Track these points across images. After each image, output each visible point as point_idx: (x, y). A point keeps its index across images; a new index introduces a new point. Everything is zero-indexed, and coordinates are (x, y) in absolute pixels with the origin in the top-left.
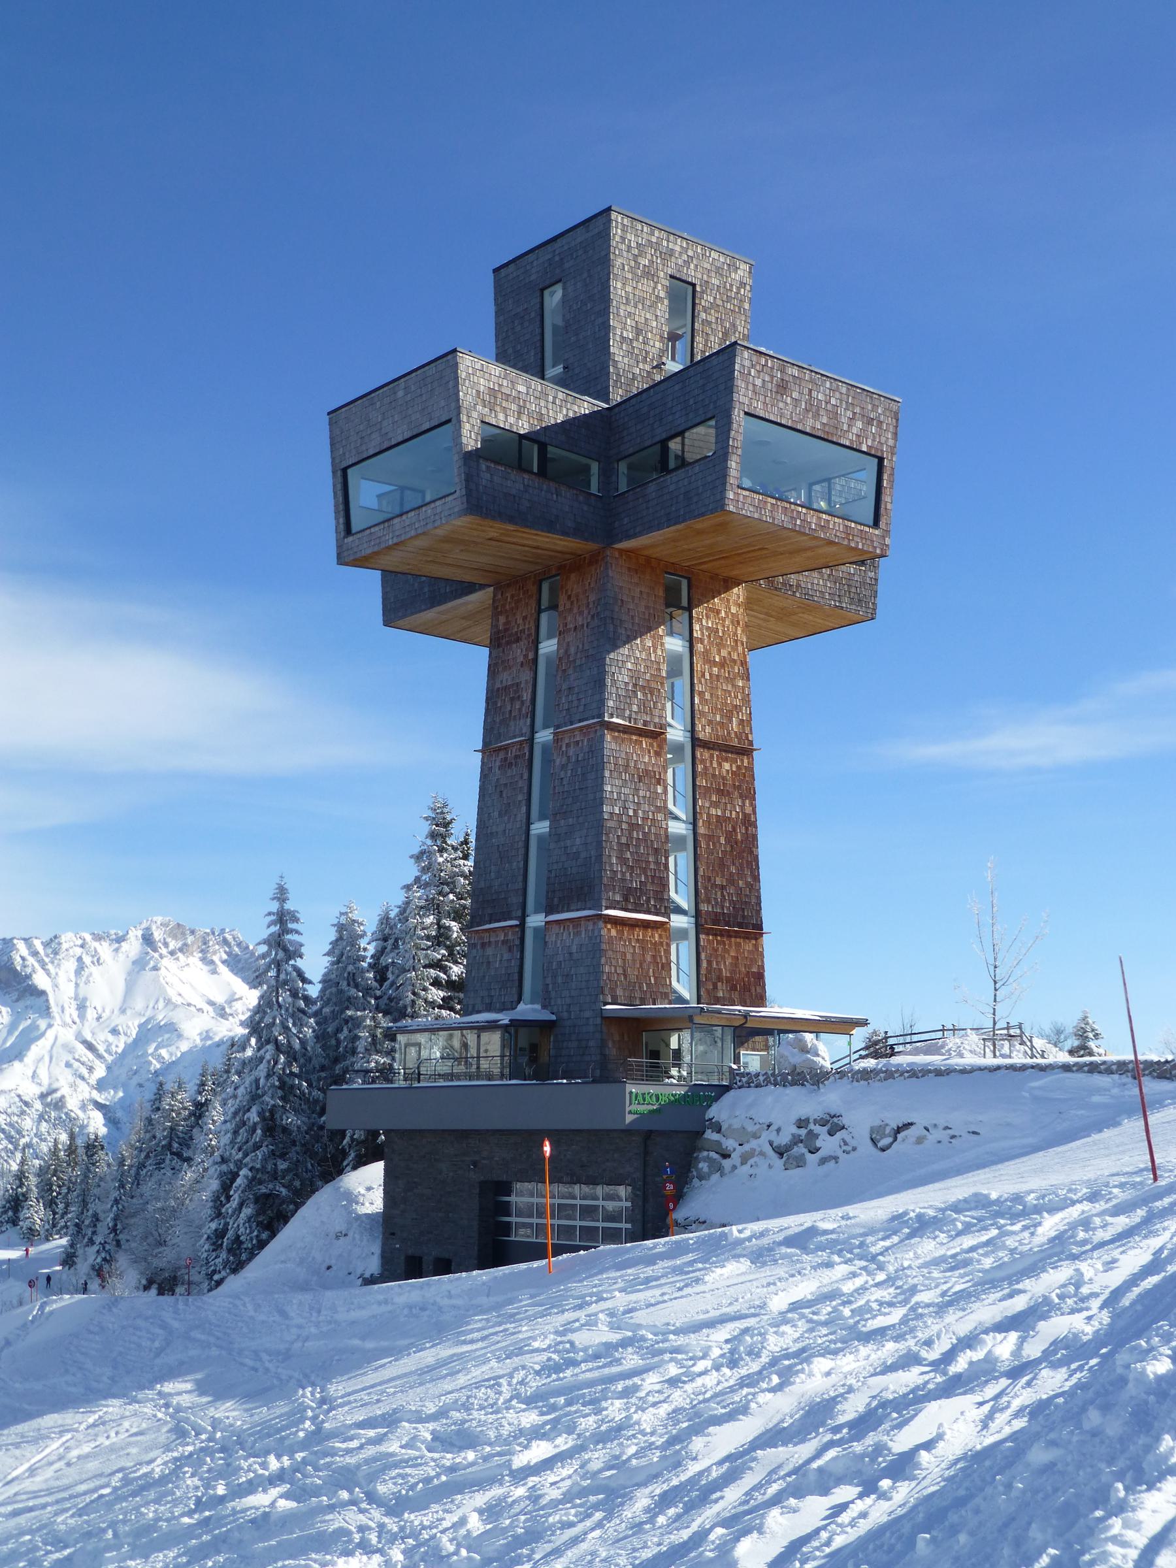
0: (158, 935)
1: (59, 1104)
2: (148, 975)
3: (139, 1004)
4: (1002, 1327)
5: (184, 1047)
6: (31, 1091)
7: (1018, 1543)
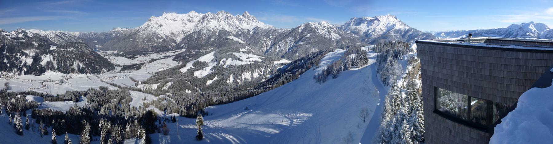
0: (389, 16)
1: (382, 29)
2: (388, 19)
3: (387, 21)
4: (299, 63)
5: (391, 25)
6: (379, 28)
7: (287, 68)
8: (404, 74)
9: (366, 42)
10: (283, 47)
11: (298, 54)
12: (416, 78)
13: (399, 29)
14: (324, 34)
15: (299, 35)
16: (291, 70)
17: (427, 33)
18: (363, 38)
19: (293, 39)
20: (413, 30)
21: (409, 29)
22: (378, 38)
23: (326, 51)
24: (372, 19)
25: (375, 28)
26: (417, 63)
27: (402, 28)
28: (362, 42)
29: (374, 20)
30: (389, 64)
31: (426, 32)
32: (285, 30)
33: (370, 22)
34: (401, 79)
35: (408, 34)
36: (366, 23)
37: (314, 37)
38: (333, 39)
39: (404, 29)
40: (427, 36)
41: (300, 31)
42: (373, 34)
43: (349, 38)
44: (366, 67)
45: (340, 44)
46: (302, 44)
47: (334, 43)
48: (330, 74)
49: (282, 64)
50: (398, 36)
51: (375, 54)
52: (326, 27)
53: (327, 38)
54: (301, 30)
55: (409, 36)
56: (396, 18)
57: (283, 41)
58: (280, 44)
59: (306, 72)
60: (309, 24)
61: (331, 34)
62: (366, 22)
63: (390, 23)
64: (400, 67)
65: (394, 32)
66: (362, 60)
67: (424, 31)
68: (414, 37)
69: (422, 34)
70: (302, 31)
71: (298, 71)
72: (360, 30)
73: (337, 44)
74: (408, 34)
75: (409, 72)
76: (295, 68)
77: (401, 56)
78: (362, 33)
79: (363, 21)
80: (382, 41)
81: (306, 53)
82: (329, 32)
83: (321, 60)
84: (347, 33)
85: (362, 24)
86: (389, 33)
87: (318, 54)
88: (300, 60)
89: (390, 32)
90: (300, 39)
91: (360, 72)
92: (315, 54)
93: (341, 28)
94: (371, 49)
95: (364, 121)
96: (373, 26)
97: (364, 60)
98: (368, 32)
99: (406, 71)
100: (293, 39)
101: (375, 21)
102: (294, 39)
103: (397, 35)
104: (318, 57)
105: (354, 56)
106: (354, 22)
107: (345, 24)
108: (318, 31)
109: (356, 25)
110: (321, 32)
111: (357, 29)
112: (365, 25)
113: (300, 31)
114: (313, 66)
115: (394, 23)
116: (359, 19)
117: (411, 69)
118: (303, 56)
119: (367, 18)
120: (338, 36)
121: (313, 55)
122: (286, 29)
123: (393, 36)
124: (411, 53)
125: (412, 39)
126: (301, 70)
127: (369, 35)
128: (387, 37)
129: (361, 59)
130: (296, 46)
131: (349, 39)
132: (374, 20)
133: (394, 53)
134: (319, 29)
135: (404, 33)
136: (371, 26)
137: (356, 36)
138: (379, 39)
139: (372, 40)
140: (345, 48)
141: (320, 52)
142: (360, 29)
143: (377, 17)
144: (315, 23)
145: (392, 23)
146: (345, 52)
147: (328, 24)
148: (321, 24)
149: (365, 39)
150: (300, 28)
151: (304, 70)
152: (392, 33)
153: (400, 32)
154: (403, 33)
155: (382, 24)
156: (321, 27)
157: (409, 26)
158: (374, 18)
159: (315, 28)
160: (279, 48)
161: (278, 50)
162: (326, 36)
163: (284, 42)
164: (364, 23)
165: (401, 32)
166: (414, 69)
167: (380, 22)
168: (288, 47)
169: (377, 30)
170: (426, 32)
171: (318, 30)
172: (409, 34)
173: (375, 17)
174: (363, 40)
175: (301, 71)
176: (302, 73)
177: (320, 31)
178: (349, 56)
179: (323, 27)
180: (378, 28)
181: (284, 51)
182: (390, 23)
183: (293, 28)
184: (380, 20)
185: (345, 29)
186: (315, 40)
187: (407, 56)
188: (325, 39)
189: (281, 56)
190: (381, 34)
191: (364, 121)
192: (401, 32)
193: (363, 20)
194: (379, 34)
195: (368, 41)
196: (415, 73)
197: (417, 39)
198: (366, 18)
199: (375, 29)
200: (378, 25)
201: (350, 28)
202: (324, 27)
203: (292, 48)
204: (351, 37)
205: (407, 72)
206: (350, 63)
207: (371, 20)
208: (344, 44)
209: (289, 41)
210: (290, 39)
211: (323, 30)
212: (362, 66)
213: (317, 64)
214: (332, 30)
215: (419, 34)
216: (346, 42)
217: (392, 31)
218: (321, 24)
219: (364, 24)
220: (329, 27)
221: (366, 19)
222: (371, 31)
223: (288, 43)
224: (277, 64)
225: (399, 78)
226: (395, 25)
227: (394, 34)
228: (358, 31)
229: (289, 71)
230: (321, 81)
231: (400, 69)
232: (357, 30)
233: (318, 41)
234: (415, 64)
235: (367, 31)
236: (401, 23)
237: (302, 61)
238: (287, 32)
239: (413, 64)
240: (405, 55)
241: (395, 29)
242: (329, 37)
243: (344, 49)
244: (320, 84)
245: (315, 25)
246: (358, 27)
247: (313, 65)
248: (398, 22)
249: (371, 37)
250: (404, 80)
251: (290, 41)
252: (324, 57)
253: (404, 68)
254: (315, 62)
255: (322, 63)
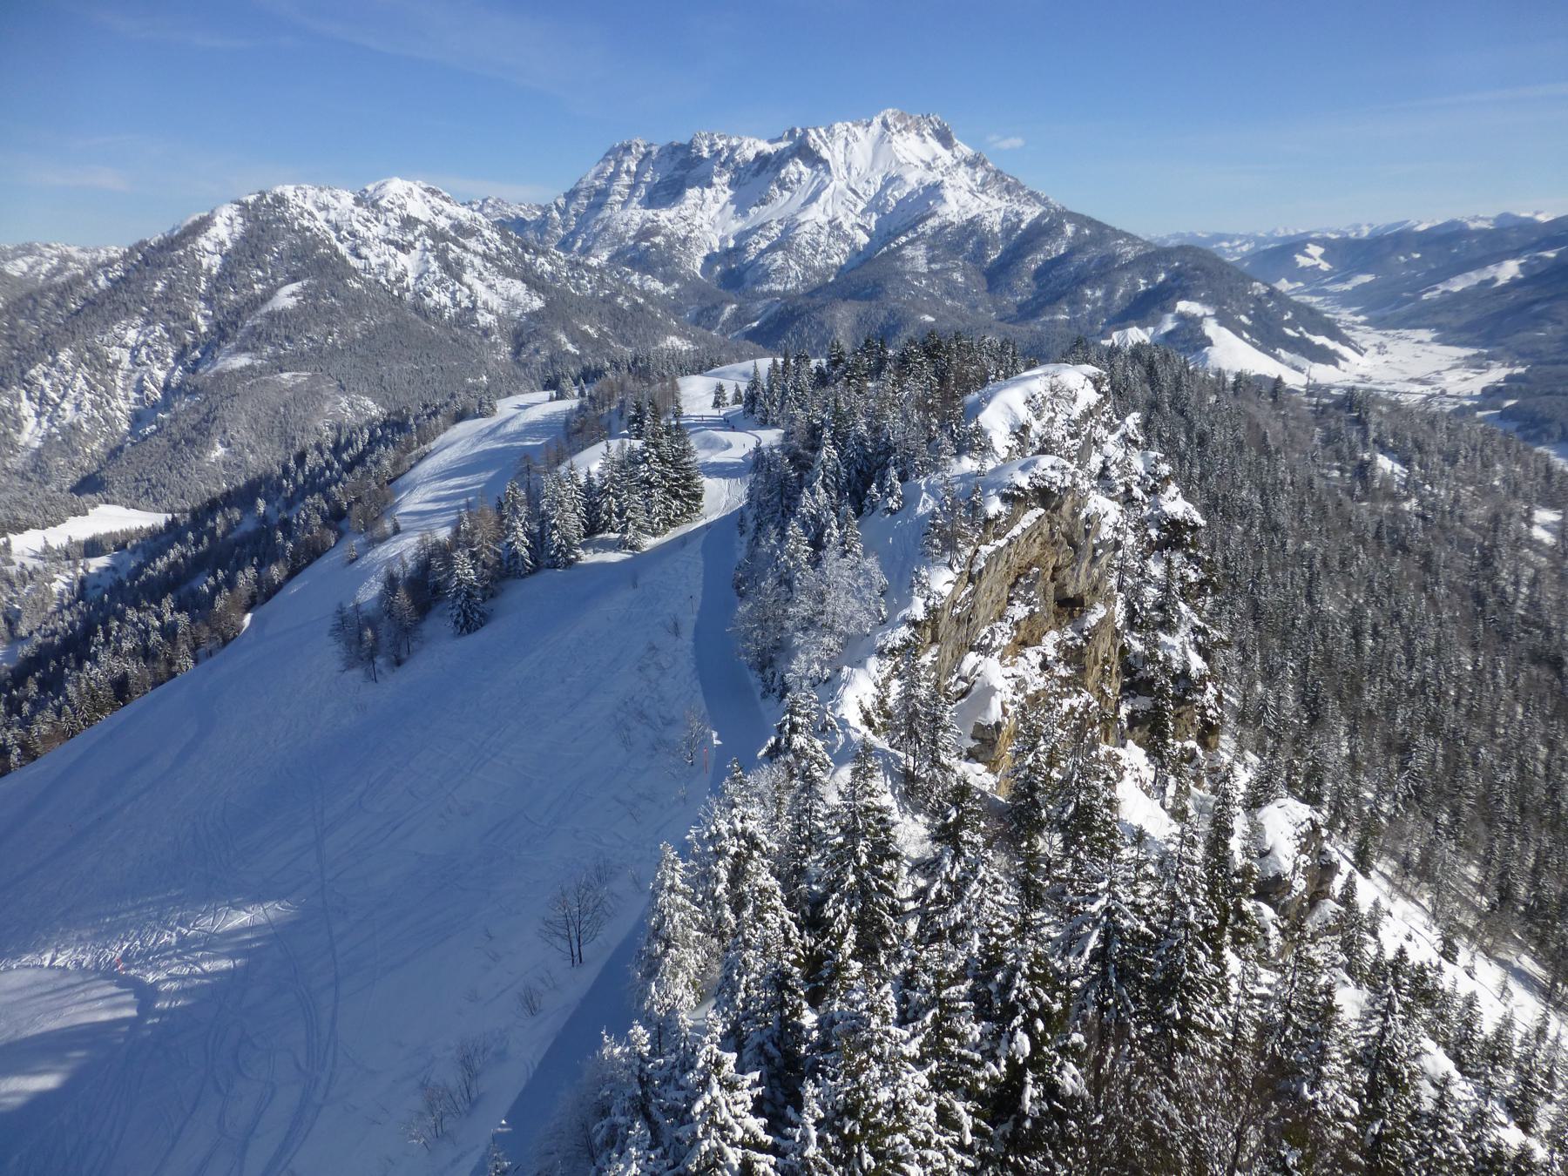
0: (890, 121)
1: (839, 227)
2: (886, 145)
6: (823, 219)
8: (895, 627)
9: (727, 328)
10: (78, 407)
11: (219, 452)
12: (984, 650)
13: (971, 221)
14: (410, 280)
15: (208, 300)
16: (175, 581)
17: (1182, 249)
18: (703, 296)
19: (159, 329)
20: (1069, 229)
21: (1042, 216)
22: (812, 293)
23: (435, 413)
24: (769, 148)
25: (793, 218)
26: (1002, 543)
27: (992, 210)
28: (701, 331)
29: (780, 160)
30: (797, 550)
31: (1172, 243)
32: (65, 259)
33: (758, 173)
34: (873, 663)
35: (1035, 260)
36: (721, 180)
37: (332, 310)
38: (485, 319)
39: (1005, 219)
40: (1176, 275)
41: (205, 262)
42: (780, 262)
43: (604, 300)
44: (683, 541)
45: (537, 351)
46: (241, 370)
47: (494, 345)
48: (438, 601)
49: (92, 547)
50: (958, 277)
51: (761, 433)
52: (417, 221)
53: (439, 310)
54: (217, 259)
55: (1039, 274)
56: (945, 138)
57: (65, 356)
58: (47, 384)
59: (294, 588)
60: (280, 200)
61: (467, 278)
62: (726, 178)
63: (899, 178)
64: (867, 572)
65: (930, 248)
66: (657, 494)
67: (1164, 235)
68: (1081, 280)
69: (1138, 261)
70: (223, 266)
71: (230, 583)
72: (685, 241)
73: (517, 353)
74: (1035, 260)
75: (932, 612)
76: (198, 565)
77: (892, 485)
78: (699, 262)
79: (699, 171)
80: (844, 323)
81: (284, 433)
82: (446, 267)
83: (401, 482)
84: (589, 269)
85: (692, 194)
86: (895, 254)
87: (373, 442)
88: (242, 497)
89: (901, 247)
90: (221, 332)
91: (635, 586)
92: (349, 443)
93: (542, 225)
94: (736, 401)
95: (577, 959)
96: (782, 203)
97: (668, 491)
98: (739, 250)
99: (908, 603)
100: (159, 329)
101: (791, 168)
102: (167, 330)
103: (953, 270)
104: (377, 463)
105: (595, 468)
106: (638, 175)
107: (571, 195)
108: (359, 256)
109: (651, 201)
110: (385, 265)
111: (656, 230)
112: (716, 200)
113: (212, 262)
114: (341, 535)
115: (931, 178)
116: (673, 150)
117: (947, 590)
118: (263, 459)
119: (734, 142)
120: (518, 288)
121: (337, 449)
122: (73, 251)
123: (918, 275)
124: (968, 464)
125: (1064, 294)
126: (250, 572)
127: (748, 275)
128: (876, 285)
129: (651, 486)
130: (196, 390)
131: (606, 309)
132: (780, 160)
133: (849, 463)
134: (365, 242)
135: (1006, 252)
136: (763, 202)
137: (656, 285)
138: (818, 300)
139: (774, 309)
140: (567, 384)
141: (385, 425)
142: (682, 233)
143: (805, 133)
144: (326, 197)
145: (913, 179)
146: (571, 412)
147: (436, 201)
148: (383, 203)
149: (718, 307)
150: (202, 241)
151: (276, 572)
152: (917, 257)
153: (970, 246)
154: (993, 255)
155: (842, 185)
156: (379, 230)
157: (1042, 193)
158: (782, 145)
159: (333, 235)
160: (39, 415)
161: (31, 433)
162: (429, 295)
163: (78, 361)
164: (710, 185)
165: (982, 244)
166: (970, 588)
167: (828, 170)
168: (122, 406)
169: (803, 236)
170: (1176, 236)
171: (364, 251)
172: (1041, 256)
173: (792, 132)
174: (706, 316)
175: (258, 581)
176: (264, 594)
177: (374, 261)
178: (563, 469)
179: (394, 224)
180: (816, 214)
181: (94, 438)
182: (899, 178)
183: (143, 243)
184: (825, 153)
185: (574, 234)
186: (341, 333)
187: (931, 490)
188: (426, 318)
189: (71, 479)
190: (836, 260)
191: (577, 959)
192: (982, 244)
193: (701, 159)
194: (818, 262)
195: (739, 318)
196: (982, 612)
197: (1099, 293)
198: (721, 144)
199: (790, 226)
200: (814, 197)
201: (605, 229)
202: (409, 223)
203: (166, 405)
204: (617, 293)
205: (918, 611)
206: (571, 520)
207: (763, 161)
208: (570, 347)
209: (126, 356)
210: (131, 336)
211: (404, 248)
212: (654, 535)
213: (370, 523)
214: (472, 243)
215: (1113, 258)
216: (585, 333)
217: (911, 242)
218: (375, 204)
219: (709, 193)
220: (442, 223)
221: (719, 153)
222: (764, 245)
223: (115, 366)
224: (47, 553)
225: (854, 650)
226: (933, 191)
227: (930, 261)
228: (670, 246)
229: (154, 591)
230: (380, 661)
231: (870, 586)
232: (658, 240)
233: (370, 335)
234: (983, 548)
235: (731, 244)
236: (979, 175)
237: (253, 504)
238: (89, 274)
239: (969, 552)
240: (923, 481)
241: (933, 222)
242: (457, 304)
243: (561, 396)
244: (373, 677)
245: (325, 208)
246: (664, 215)
247: (343, 525)
248: (962, 169)
249: (766, 288)
250: (889, 664)
251: (135, 351)
252: (421, 459)
253: (902, 582)
254: (358, 500)
255: (412, 502)
